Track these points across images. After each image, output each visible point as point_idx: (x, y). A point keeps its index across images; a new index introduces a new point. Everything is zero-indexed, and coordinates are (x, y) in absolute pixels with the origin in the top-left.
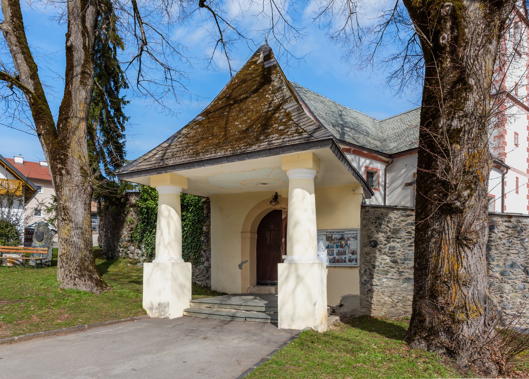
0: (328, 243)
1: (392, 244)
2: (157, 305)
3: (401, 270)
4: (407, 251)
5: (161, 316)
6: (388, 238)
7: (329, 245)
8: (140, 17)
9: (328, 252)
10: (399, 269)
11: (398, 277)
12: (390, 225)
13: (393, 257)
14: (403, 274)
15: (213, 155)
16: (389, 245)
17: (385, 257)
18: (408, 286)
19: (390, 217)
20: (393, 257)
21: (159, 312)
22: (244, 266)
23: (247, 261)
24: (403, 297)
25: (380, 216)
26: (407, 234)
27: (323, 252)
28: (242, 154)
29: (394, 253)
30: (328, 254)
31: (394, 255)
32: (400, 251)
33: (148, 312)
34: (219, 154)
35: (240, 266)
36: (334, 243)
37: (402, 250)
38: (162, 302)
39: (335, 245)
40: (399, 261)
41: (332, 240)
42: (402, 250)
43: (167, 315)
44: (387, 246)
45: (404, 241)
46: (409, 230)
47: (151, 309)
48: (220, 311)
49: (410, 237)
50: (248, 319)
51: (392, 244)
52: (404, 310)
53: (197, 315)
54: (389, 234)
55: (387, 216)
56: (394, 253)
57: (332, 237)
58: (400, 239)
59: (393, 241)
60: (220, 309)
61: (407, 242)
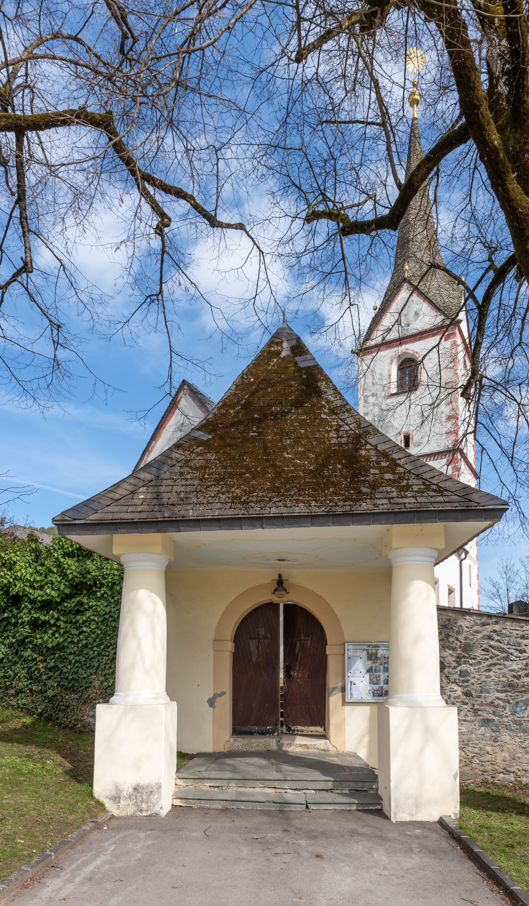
0: (369, 663)
1: (464, 667)
2: (131, 790)
3: (476, 707)
4: (483, 679)
5: (141, 811)
6: (458, 657)
7: (372, 667)
8: (26, 219)
9: (370, 679)
10: (474, 705)
11: (473, 718)
12: (461, 638)
13: (466, 687)
14: (479, 713)
15: (284, 511)
16: (459, 668)
17: (455, 687)
18: (486, 732)
19: (461, 626)
20: (466, 687)
21: (136, 804)
22: (219, 701)
23: (224, 693)
24: (481, 749)
25: (447, 623)
26: (483, 653)
27: (362, 679)
28: (345, 514)
29: (467, 681)
30: (371, 682)
31: (466, 684)
32: (474, 677)
33: (109, 805)
34: (300, 509)
35: (211, 703)
36: (381, 664)
37: (477, 677)
38: (144, 782)
39: (382, 668)
40: (473, 693)
41: (377, 658)
42: (477, 677)
43: (157, 809)
44: (456, 670)
45: (479, 663)
46: (485, 646)
47: (116, 799)
48: (246, 794)
49: (487, 657)
50: (312, 807)
51: (464, 667)
52: (482, 768)
53: (204, 804)
54: (459, 651)
55: (456, 623)
56: (467, 681)
57: (376, 654)
58: (475, 659)
59: (465, 662)
60: (242, 790)
61: (483, 665)
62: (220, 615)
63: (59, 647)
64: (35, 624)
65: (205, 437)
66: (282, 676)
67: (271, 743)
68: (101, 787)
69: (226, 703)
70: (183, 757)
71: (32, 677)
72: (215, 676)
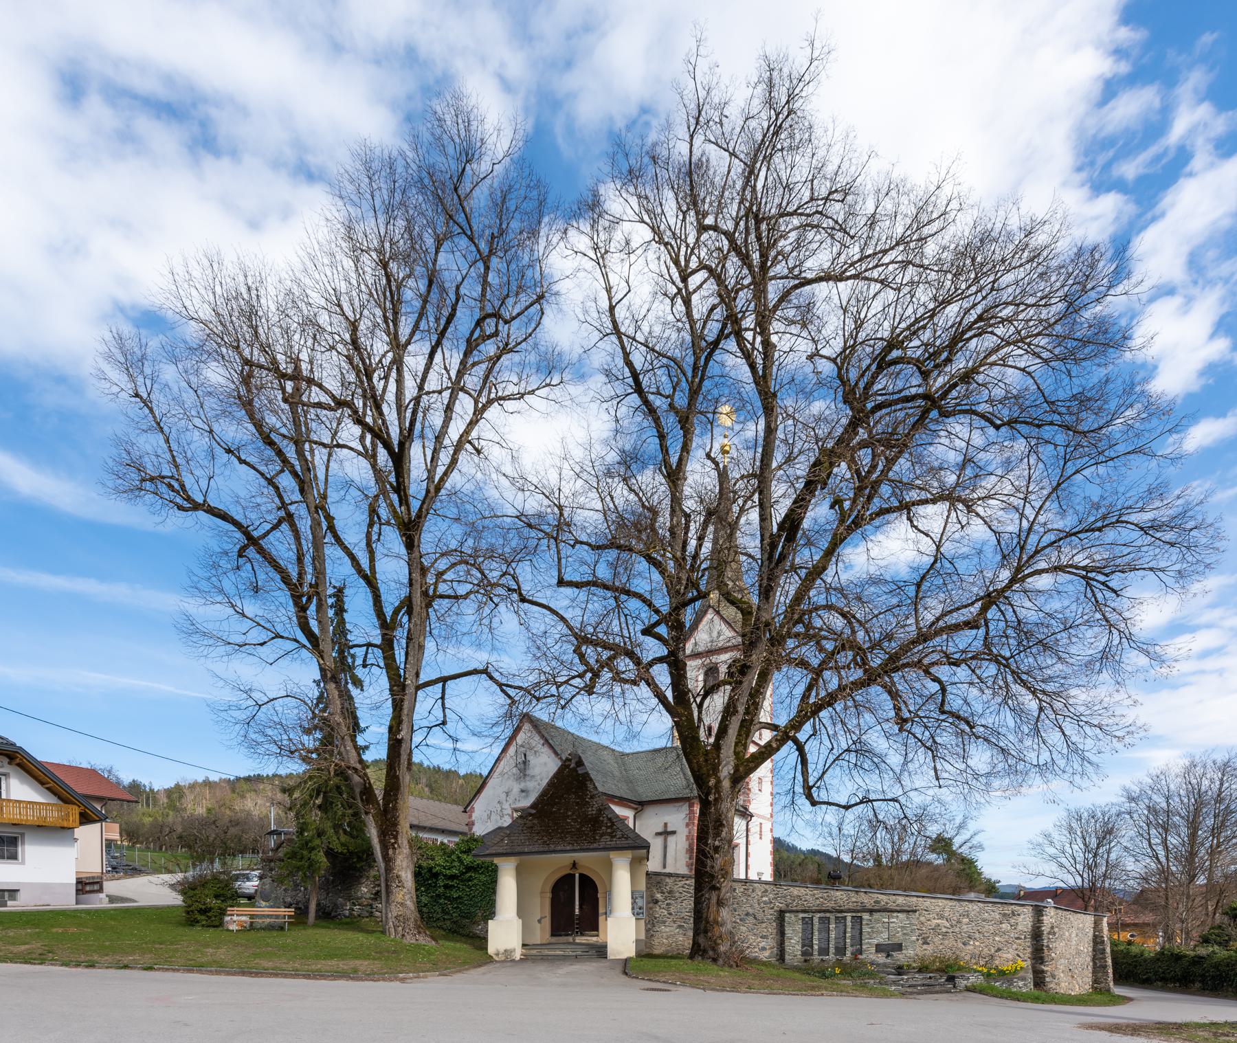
35: (539, 921)
47: (497, 954)
62: (543, 881)
63: (459, 897)
64: (446, 887)
65: (533, 811)
66: (577, 907)
67: (570, 939)
68: (491, 950)
69: (547, 922)
70: (524, 945)
71: (444, 911)
72: (541, 908)
